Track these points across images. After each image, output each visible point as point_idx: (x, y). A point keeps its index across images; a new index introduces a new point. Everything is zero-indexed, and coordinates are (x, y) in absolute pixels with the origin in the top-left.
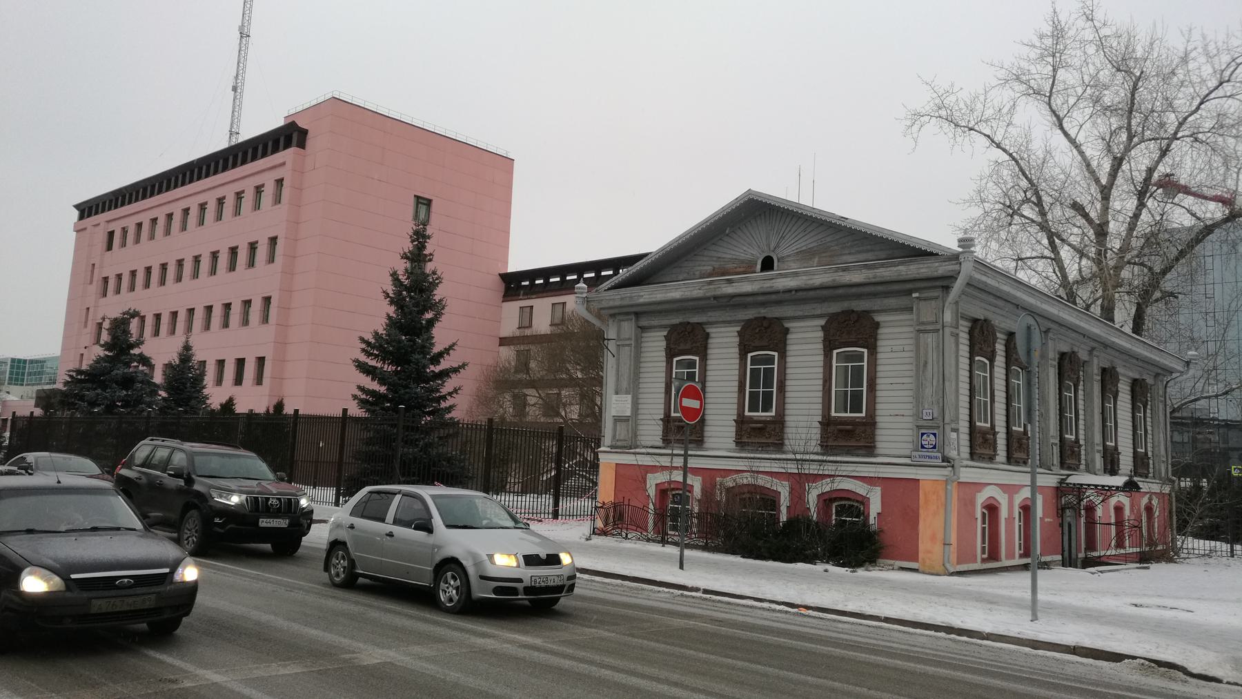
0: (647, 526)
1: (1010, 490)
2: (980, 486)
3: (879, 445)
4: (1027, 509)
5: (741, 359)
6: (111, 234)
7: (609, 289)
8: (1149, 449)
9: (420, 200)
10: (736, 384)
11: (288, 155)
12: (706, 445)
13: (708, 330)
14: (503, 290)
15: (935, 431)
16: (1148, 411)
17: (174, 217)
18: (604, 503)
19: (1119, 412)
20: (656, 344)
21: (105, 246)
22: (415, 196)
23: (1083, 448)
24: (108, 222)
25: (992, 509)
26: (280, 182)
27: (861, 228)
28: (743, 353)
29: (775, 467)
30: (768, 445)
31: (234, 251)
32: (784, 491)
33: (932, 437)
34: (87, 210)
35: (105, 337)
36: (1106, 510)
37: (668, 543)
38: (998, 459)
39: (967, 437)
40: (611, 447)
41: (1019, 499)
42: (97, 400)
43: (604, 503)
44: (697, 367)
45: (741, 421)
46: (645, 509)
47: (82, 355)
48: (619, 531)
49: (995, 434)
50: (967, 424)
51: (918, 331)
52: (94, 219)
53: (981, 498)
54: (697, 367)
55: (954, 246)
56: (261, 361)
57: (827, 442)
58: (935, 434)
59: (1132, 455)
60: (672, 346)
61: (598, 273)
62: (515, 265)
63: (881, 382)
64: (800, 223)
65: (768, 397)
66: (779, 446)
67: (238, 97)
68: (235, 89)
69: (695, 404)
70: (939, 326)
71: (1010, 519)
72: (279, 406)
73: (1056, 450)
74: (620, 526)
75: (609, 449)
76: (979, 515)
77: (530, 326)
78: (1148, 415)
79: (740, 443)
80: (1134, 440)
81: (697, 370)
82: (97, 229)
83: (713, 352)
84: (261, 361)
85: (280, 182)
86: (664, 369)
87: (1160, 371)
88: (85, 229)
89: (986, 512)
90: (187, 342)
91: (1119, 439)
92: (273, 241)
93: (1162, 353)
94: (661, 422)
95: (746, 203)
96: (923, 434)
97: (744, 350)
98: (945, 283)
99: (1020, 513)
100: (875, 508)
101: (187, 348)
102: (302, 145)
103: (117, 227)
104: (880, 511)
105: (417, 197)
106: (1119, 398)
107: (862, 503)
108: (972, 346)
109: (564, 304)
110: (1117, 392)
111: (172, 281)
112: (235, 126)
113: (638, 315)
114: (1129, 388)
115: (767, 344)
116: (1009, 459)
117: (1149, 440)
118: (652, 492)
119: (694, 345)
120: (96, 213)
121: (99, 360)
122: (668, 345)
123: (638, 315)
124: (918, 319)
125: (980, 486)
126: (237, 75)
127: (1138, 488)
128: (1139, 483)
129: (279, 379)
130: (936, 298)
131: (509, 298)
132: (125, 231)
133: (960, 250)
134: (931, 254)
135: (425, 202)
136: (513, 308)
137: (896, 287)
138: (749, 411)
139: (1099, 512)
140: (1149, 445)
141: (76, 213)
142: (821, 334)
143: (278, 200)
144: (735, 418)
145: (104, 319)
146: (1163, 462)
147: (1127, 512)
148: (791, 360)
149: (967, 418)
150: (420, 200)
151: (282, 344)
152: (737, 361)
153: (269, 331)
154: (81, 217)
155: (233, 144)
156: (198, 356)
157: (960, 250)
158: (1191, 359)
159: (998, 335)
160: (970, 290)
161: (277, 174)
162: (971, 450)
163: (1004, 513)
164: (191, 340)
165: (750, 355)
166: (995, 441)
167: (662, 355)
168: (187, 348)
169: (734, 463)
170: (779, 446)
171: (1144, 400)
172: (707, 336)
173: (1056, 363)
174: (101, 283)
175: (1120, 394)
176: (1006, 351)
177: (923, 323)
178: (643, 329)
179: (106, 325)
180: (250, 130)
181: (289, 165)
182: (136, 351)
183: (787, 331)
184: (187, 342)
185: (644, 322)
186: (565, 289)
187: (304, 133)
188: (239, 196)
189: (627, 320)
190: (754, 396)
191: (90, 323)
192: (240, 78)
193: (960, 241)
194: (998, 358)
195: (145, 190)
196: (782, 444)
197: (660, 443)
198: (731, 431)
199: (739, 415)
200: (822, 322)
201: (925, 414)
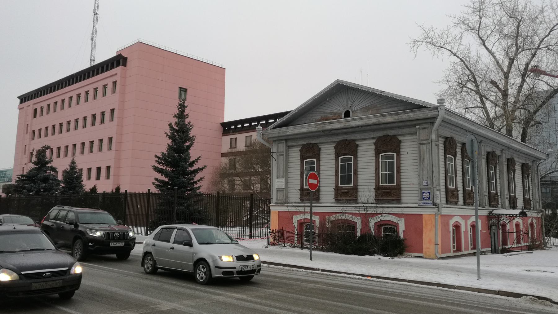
0: (294, 240)
1: (464, 217)
2: (451, 216)
3: (403, 198)
4: (474, 227)
5: (301, 163)
6: (36, 110)
8: (531, 196)
9: (182, 89)
11: (118, 70)
12: (321, 201)
13: (320, 147)
14: (222, 131)
17: (65, 101)
20: (295, 154)
21: (33, 115)
22: (179, 87)
23: (499, 197)
24: (34, 104)
25: (457, 227)
26: (115, 83)
29: (354, 211)
30: (350, 200)
31: (94, 116)
32: (358, 221)
33: (428, 194)
34: (24, 99)
35: (34, 159)
36: (511, 226)
38: (459, 203)
39: (444, 193)
40: (276, 203)
41: (470, 222)
42: (31, 189)
46: (293, 232)
47: (24, 168)
49: (457, 191)
50: (444, 187)
52: (27, 103)
53: (452, 222)
55: (435, 103)
56: (108, 168)
57: (378, 198)
58: (429, 193)
60: (303, 155)
61: (267, 121)
62: (228, 118)
64: (362, 94)
65: (349, 177)
66: (398, 200)
67: (94, 43)
68: (92, 39)
69: (314, 182)
70: (429, 141)
71: (466, 232)
72: (118, 189)
73: (487, 198)
76: (451, 230)
77: (236, 147)
79: (337, 200)
80: (523, 192)
82: (29, 108)
83: (322, 157)
84: (108, 168)
85: (115, 83)
87: (535, 159)
88: (23, 108)
90: (73, 160)
92: (113, 111)
93: (535, 151)
94: (299, 191)
95: (336, 86)
96: (423, 193)
98: (432, 121)
101: (73, 163)
102: (125, 65)
103: (38, 107)
104: (404, 230)
105: (180, 88)
106: (516, 173)
107: (396, 226)
108: (445, 150)
109: (251, 136)
111: (65, 131)
112: (93, 57)
114: (520, 168)
115: (348, 152)
118: (296, 224)
120: (28, 100)
121: (32, 170)
125: (451, 216)
126: (93, 33)
127: (526, 215)
129: (117, 176)
131: (225, 134)
132: (42, 108)
133: (438, 105)
134: (427, 107)
135: (184, 90)
136: (227, 139)
137: (408, 123)
138: (341, 184)
139: (508, 227)
140: (531, 194)
141: (19, 101)
143: (114, 91)
144: (374, 187)
145: (33, 150)
148: (403, 156)
149: (444, 184)
150: (182, 89)
151: (118, 159)
152: (334, 161)
153: (113, 153)
154: (21, 102)
155: (92, 65)
156: (79, 166)
157: (438, 105)
159: (458, 144)
161: (113, 79)
163: (463, 229)
164: (75, 159)
168: (73, 163)
169: (335, 209)
170: (355, 200)
172: (320, 149)
173: (485, 157)
174: (31, 133)
176: (462, 152)
177: (422, 140)
178: (289, 147)
179: (35, 153)
180: (100, 58)
181: (119, 74)
182: (49, 165)
184: (73, 160)
185: (289, 144)
187: (125, 59)
188: (96, 90)
189: (282, 143)
191: (27, 152)
192: (94, 34)
193: (438, 100)
195: (51, 88)
196: (357, 200)
197: (299, 201)
198: (332, 194)
200: (374, 141)
201: (424, 183)
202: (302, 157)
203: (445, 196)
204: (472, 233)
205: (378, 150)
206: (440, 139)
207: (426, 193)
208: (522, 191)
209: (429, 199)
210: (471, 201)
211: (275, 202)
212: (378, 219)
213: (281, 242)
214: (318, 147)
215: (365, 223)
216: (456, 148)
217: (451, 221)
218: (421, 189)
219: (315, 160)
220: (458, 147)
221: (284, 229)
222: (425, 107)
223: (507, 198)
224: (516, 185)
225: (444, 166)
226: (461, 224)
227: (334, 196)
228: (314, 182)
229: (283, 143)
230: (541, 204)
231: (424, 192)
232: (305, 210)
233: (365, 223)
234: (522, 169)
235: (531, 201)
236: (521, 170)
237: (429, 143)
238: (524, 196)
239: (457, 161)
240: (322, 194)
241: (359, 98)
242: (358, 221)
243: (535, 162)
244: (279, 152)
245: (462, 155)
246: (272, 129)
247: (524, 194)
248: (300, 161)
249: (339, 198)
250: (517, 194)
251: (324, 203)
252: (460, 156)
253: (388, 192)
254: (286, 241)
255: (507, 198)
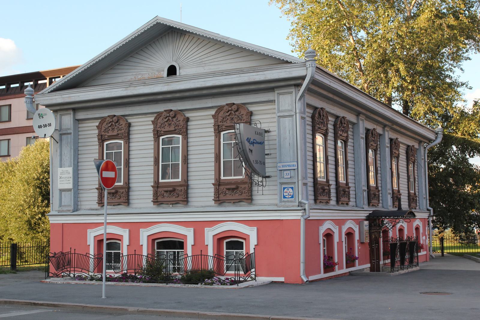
0: (89, 267)
1: (339, 223)
2: (320, 222)
4: (350, 235)
5: (155, 141)
7: (52, 91)
8: (417, 190)
10: (152, 159)
13: (130, 121)
15: (292, 186)
16: (416, 166)
18: (55, 254)
19: (400, 167)
23: (380, 192)
25: (329, 236)
27: (242, 45)
28: (217, 131)
30: (240, 201)
32: (189, 234)
33: (291, 190)
36: (394, 233)
37: (18, 271)
38: (350, 203)
39: (312, 189)
41: (344, 229)
43: (55, 254)
44: (231, 142)
45: (157, 186)
46: (87, 255)
48: (68, 273)
49: (329, 185)
50: (312, 180)
51: (279, 116)
53: (323, 230)
54: (231, 142)
58: (292, 188)
59: (407, 195)
60: (103, 133)
63: (133, 162)
64: (195, 39)
65: (175, 167)
66: (186, 201)
69: (106, 174)
70: (293, 113)
71: (340, 243)
73: (365, 194)
74: (69, 269)
75: (57, 213)
76: (321, 241)
77: (10, 120)
78: (416, 169)
80: (408, 185)
81: (122, 151)
83: (135, 137)
86: (213, 142)
89: (325, 239)
91: (400, 185)
94: (152, 189)
95: (154, 25)
96: (284, 188)
97: (157, 135)
98: (299, 82)
99: (345, 238)
100: (253, 241)
104: (193, 244)
106: (400, 159)
107: (120, 240)
108: (313, 127)
109: (10, 105)
110: (399, 154)
113: (75, 110)
115: (173, 129)
116: (338, 201)
117: (416, 185)
119: (119, 132)
122: (216, 122)
123: (75, 110)
124: (278, 108)
125: (320, 222)
127: (415, 216)
128: (415, 213)
130: (291, 93)
134: (291, 63)
137: (263, 86)
139: (391, 234)
140: (417, 188)
142: (212, 121)
144: (213, 182)
146: (424, 198)
147: (406, 232)
148: (133, 145)
149: (312, 176)
158: (438, 131)
159: (330, 118)
160: (313, 87)
162: (315, 197)
163: (336, 239)
165: (161, 138)
166: (329, 190)
167: (95, 140)
171: (414, 159)
172: (129, 125)
173: (364, 136)
175: (401, 156)
176: (334, 130)
177: (282, 111)
178: (78, 121)
183: (188, 120)
185: (81, 115)
186: (11, 94)
189: (66, 114)
190: (165, 167)
194: (330, 134)
196: (252, 200)
198: (150, 193)
199: (155, 182)
200: (213, 112)
201: (285, 174)
202: (101, 138)
203: (312, 193)
204: (346, 245)
205: (218, 126)
206: (308, 110)
207: (288, 189)
208: (407, 183)
209: (292, 197)
210: (345, 199)
211: (57, 209)
212: (99, 231)
213: (68, 271)
214: (127, 121)
215: (134, 237)
216: (327, 124)
217: (321, 227)
218: (282, 184)
219: (122, 142)
220: (330, 122)
221: (73, 252)
222: (287, 62)
223: (390, 194)
224: (400, 176)
225: (311, 150)
226: (334, 232)
227: (152, 197)
228: (106, 174)
229: (70, 114)
230: (428, 201)
231: (285, 188)
232: (106, 220)
233: (134, 237)
234: (407, 153)
235: (416, 197)
236: (405, 155)
237: (293, 115)
238: (409, 191)
239: (329, 142)
240: (134, 195)
241: (189, 47)
242: (125, 233)
243: (422, 144)
244: (282, 111)
245: (334, 134)
246: (52, 91)
247: (408, 188)
248: (153, 139)
249: (160, 199)
250: (400, 188)
251: (136, 208)
252: (333, 135)
253: (171, 191)
254: (76, 269)
255: (390, 194)
